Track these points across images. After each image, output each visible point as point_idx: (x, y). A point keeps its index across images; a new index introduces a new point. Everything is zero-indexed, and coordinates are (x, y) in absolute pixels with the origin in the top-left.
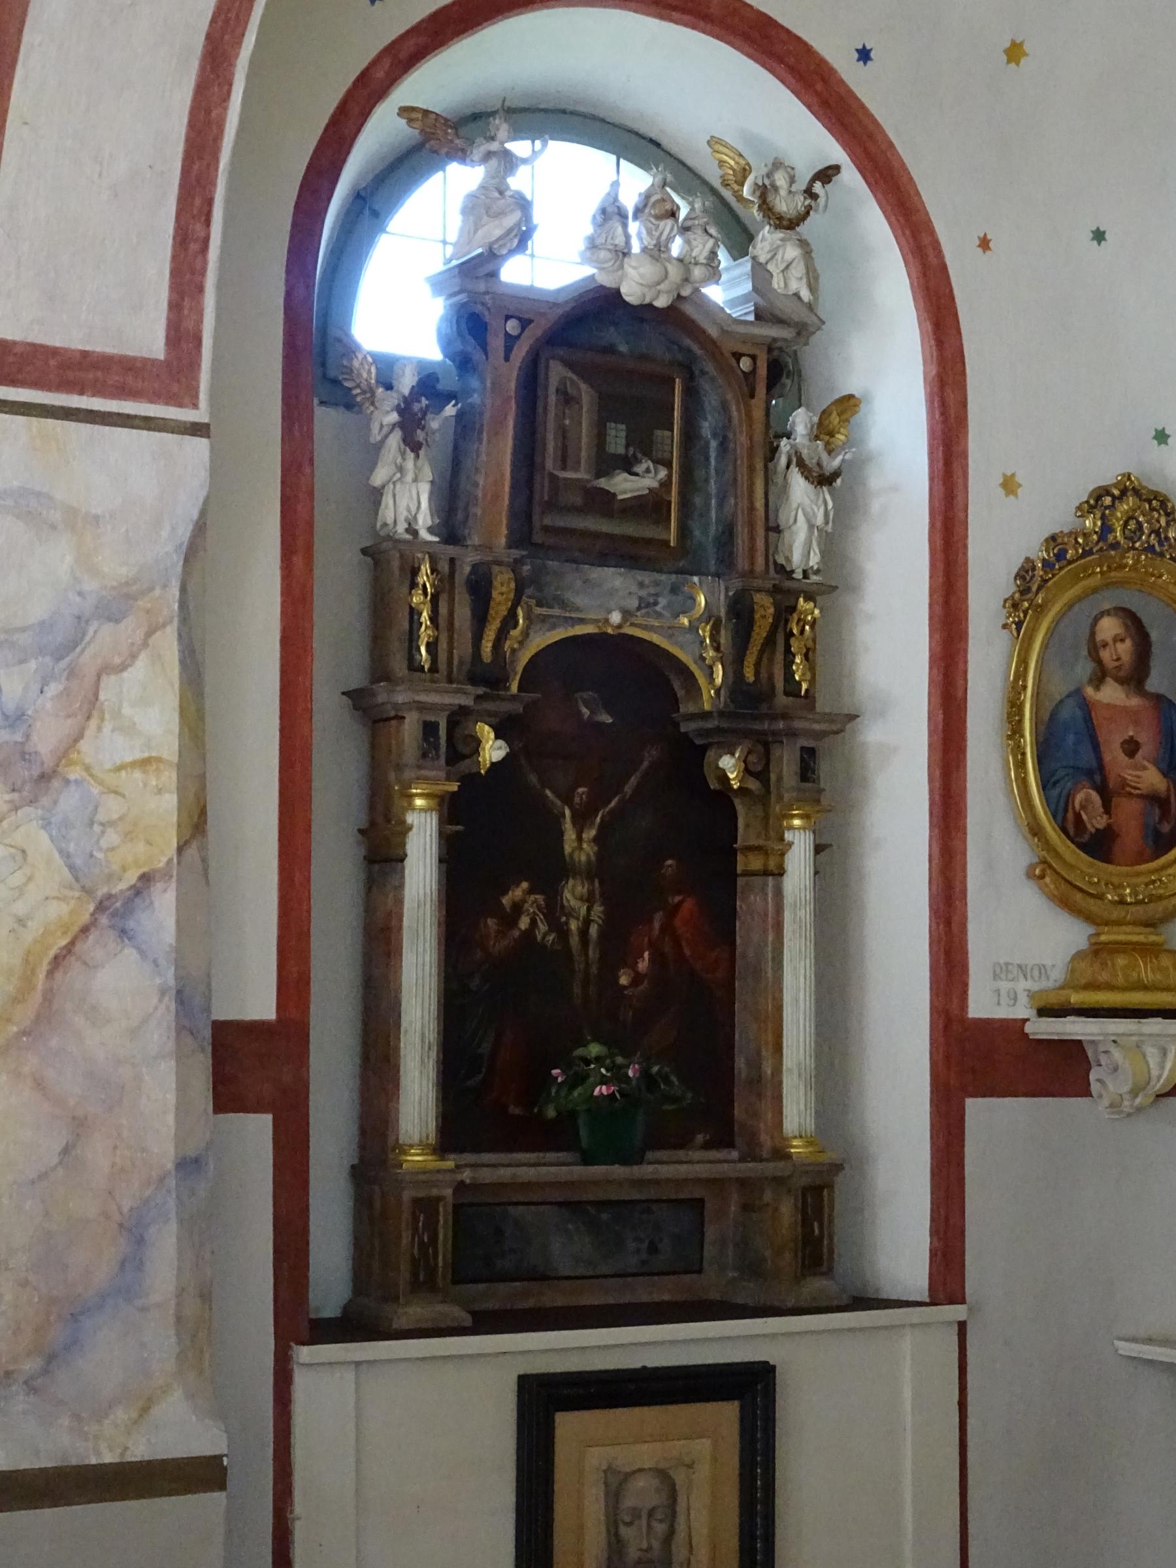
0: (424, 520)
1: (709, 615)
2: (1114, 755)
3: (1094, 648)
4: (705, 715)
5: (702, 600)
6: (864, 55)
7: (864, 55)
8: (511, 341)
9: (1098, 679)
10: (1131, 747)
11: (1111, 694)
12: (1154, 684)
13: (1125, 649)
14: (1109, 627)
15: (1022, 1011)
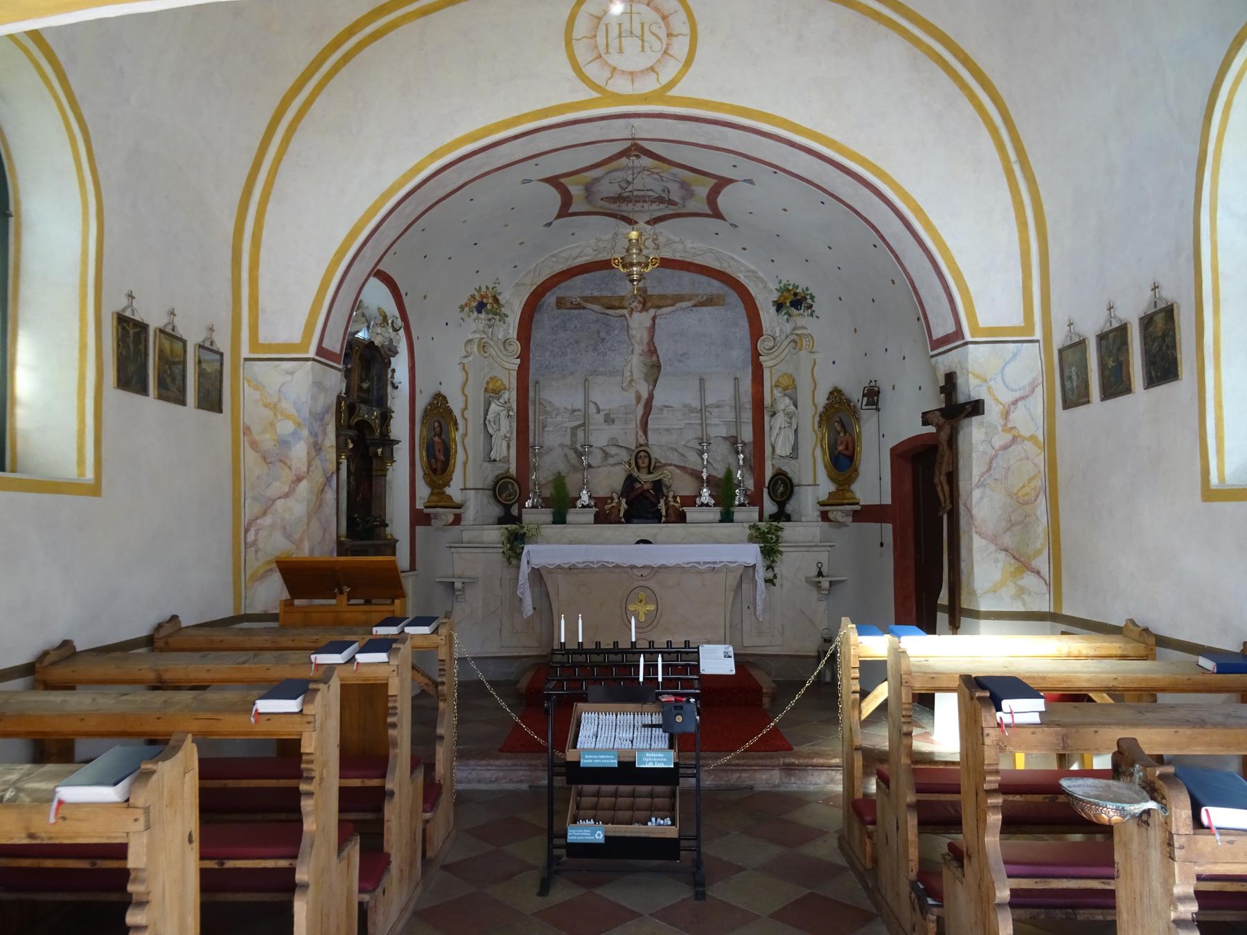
0: (344, 391)
1: (376, 417)
2: (437, 452)
3: (434, 429)
4: (377, 439)
5: (375, 413)
6: (406, 294)
7: (406, 294)
8: (357, 351)
9: (435, 436)
10: (439, 451)
11: (436, 439)
12: (443, 437)
13: (438, 429)
14: (436, 424)
15: (422, 508)
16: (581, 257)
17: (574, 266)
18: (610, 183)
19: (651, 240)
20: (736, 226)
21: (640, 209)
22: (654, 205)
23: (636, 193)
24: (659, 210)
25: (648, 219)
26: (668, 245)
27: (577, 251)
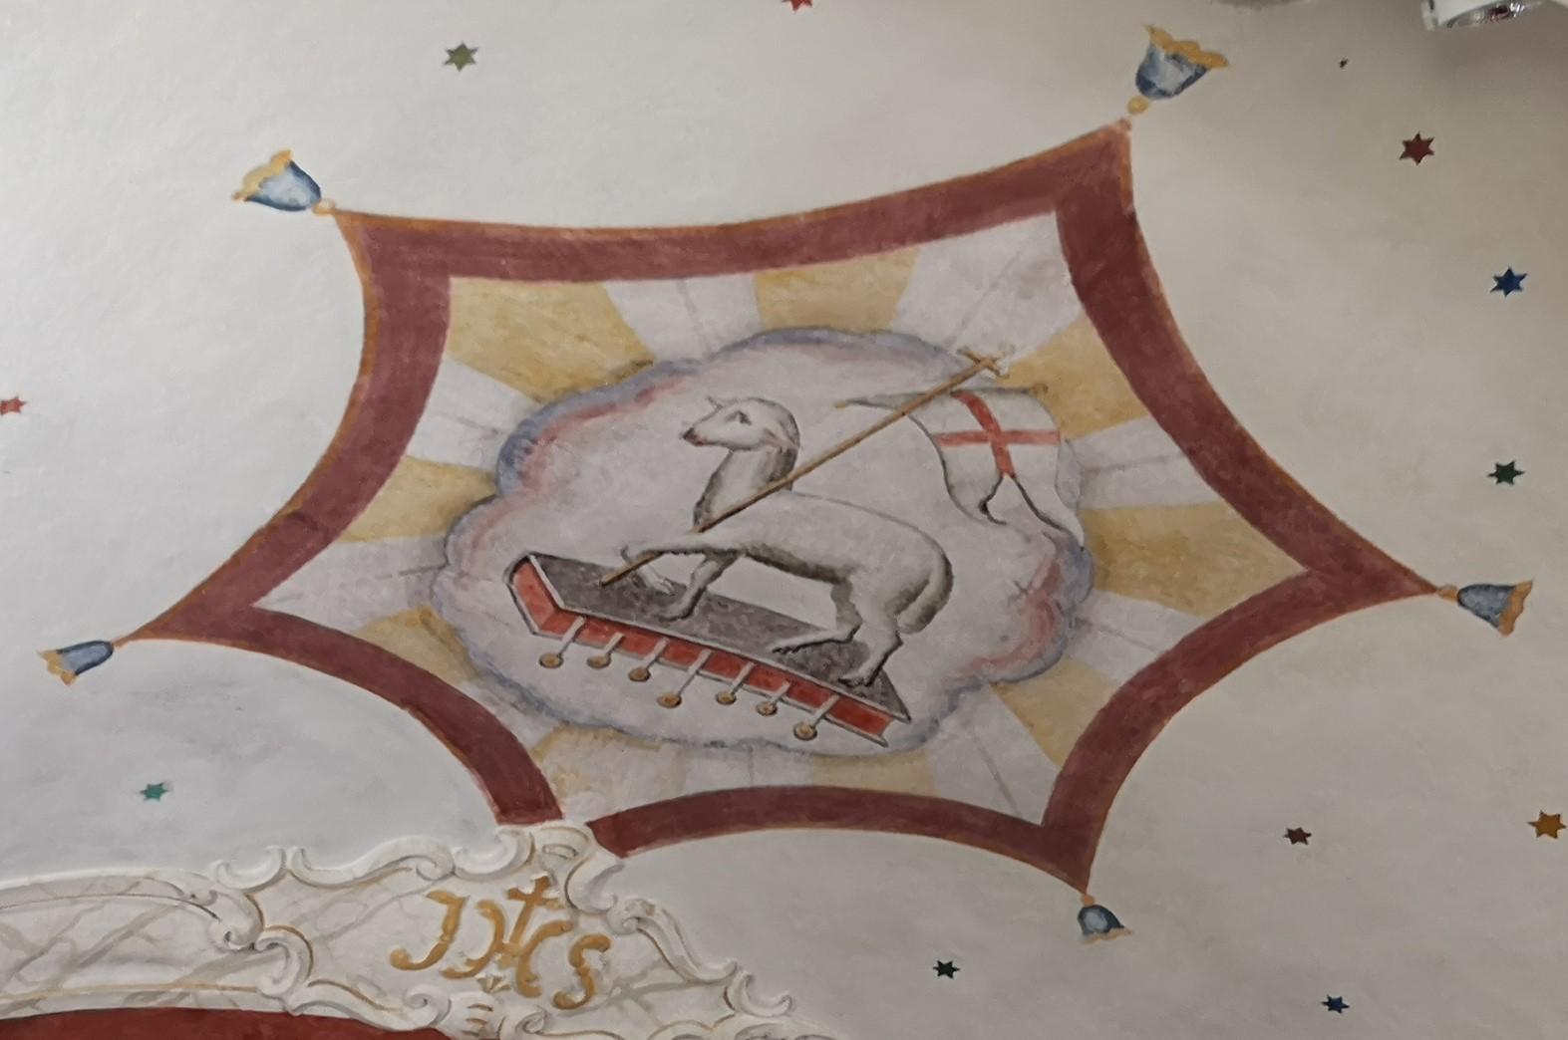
16: (125, 960)
17: (49, 1007)
18: (690, 436)
19: (564, 943)
20: (1113, 922)
21: (631, 712)
22: (749, 698)
23: (744, 582)
24: (747, 747)
25: (624, 800)
26: (637, 996)
27: (128, 911)
